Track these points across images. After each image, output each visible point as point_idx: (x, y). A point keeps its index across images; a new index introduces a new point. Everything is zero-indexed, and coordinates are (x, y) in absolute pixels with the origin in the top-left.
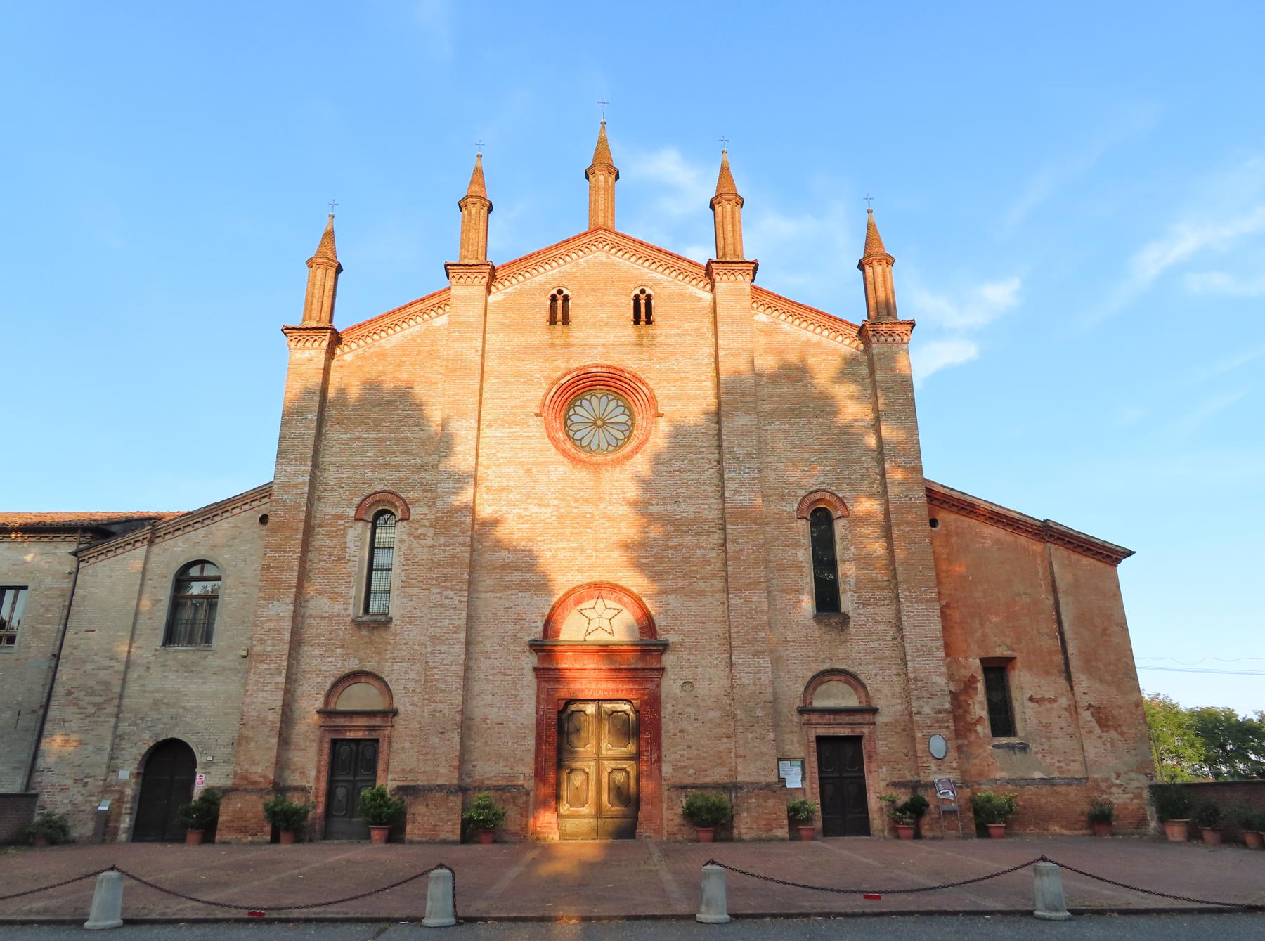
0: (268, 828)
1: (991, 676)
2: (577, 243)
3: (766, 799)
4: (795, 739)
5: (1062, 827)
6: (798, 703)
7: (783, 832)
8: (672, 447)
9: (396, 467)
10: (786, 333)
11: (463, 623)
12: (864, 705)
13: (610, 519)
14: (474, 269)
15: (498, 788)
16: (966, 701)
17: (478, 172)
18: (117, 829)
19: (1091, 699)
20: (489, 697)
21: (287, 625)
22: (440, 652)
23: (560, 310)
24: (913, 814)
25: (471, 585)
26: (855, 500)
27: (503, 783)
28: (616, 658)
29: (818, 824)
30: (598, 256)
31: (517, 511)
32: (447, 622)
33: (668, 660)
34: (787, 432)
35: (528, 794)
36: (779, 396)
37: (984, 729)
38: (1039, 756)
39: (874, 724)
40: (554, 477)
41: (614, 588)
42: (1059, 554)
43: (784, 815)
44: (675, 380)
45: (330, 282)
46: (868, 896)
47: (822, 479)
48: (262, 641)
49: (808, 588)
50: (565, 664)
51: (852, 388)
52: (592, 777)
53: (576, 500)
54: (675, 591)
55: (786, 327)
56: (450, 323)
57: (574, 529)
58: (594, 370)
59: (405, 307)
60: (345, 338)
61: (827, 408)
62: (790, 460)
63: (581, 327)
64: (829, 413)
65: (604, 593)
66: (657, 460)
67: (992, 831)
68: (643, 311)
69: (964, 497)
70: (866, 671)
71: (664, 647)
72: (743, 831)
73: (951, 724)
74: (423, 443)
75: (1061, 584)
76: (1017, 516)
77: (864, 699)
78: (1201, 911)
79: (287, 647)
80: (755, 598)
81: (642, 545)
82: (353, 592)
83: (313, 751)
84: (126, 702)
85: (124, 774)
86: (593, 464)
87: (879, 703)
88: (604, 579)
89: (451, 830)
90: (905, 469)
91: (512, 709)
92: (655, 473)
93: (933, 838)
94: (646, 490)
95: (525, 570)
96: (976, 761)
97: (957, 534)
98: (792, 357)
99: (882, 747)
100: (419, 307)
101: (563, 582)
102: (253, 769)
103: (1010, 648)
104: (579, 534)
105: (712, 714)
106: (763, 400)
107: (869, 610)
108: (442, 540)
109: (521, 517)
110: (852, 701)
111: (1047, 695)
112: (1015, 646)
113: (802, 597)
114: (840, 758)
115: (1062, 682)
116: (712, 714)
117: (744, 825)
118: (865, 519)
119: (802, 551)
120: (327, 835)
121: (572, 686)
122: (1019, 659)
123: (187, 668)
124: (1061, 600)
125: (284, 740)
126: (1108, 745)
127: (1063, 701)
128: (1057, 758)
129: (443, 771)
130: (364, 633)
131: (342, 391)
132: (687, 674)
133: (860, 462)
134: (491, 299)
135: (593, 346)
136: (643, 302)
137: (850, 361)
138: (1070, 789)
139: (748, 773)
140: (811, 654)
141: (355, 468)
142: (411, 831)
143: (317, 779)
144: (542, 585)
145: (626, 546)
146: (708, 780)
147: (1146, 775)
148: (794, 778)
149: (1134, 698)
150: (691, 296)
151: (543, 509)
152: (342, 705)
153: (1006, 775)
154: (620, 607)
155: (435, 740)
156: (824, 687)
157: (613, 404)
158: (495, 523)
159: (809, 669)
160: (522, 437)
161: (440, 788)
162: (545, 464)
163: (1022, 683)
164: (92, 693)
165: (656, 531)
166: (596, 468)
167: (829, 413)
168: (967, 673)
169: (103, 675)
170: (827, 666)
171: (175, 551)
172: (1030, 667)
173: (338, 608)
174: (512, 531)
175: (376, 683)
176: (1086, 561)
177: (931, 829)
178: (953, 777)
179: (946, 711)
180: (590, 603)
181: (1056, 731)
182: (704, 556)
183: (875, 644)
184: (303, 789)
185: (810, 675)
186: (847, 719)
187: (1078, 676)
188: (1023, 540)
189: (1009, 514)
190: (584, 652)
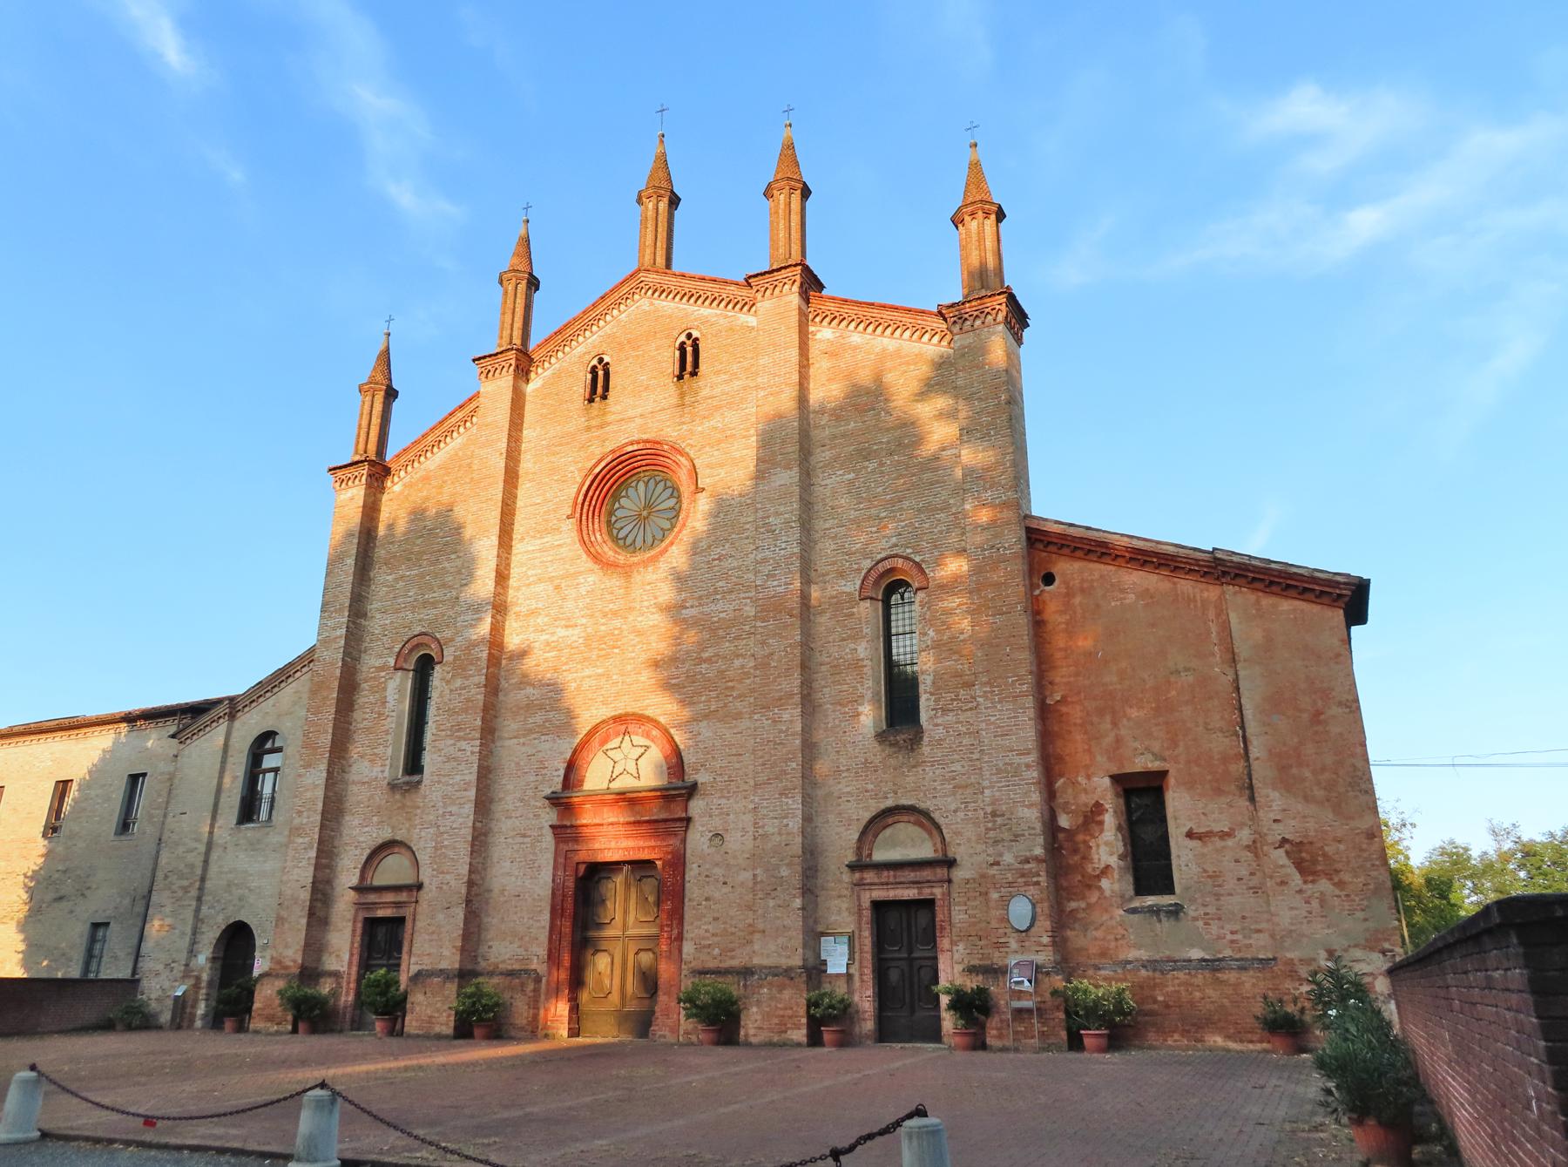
0: (290, 1018)
1: (1136, 800)
3: (781, 988)
4: (845, 906)
5: (1228, 1037)
6: (850, 857)
7: (800, 1035)
8: (713, 529)
9: (434, 605)
10: (855, 348)
11: (473, 777)
12: (939, 855)
13: (639, 633)
14: (501, 358)
15: (511, 974)
16: (1085, 842)
18: (193, 1015)
19: (1289, 830)
22: (451, 814)
23: (599, 383)
24: (973, 1007)
26: (938, 562)
27: (517, 967)
28: (638, 808)
29: (869, 1025)
31: (545, 637)
32: (458, 778)
33: (696, 806)
34: (851, 482)
35: (538, 980)
36: (843, 436)
37: (1116, 885)
38: (1200, 924)
39: (950, 881)
40: (583, 591)
41: (640, 719)
42: (1239, 600)
43: (802, 1011)
44: (720, 442)
47: (894, 540)
48: (300, 813)
49: (869, 695)
50: (585, 819)
51: (941, 402)
52: (618, 960)
54: (706, 716)
55: (856, 338)
58: (630, 448)
59: (446, 419)
61: (907, 434)
62: (853, 521)
64: (906, 446)
66: (695, 550)
67: (1087, 1041)
68: (689, 360)
69: (1090, 534)
70: (943, 806)
71: (692, 790)
72: (752, 1032)
73: (1043, 879)
75: (1242, 650)
76: (1171, 550)
77: (939, 846)
79: (319, 818)
80: (786, 717)
81: (674, 660)
84: (208, 884)
87: (958, 851)
88: (630, 710)
89: (446, 1024)
90: (993, 506)
91: (526, 878)
92: (694, 567)
93: (1004, 1049)
94: (680, 590)
95: (551, 704)
96: (1099, 934)
97: (1082, 590)
98: (864, 377)
99: (959, 916)
100: (460, 415)
101: (589, 715)
103: (1157, 757)
104: (607, 656)
107: (950, 717)
108: (458, 683)
109: (548, 644)
110: (926, 851)
111: (1216, 828)
112: (1167, 753)
113: (861, 709)
115: (1244, 803)
117: (753, 1024)
118: (948, 587)
119: (864, 644)
121: (591, 846)
122: (1172, 773)
123: (253, 846)
124: (1242, 673)
126: (1315, 904)
127: (1245, 835)
128: (1228, 927)
129: (446, 953)
130: (398, 797)
132: (717, 823)
135: (631, 419)
137: (942, 365)
138: (1245, 976)
140: (870, 787)
141: (397, 611)
142: (411, 1023)
143: (350, 964)
144: (566, 724)
145: (656, 664)
146: (735, 963)
147: (1384, 952)
148: (837, 959)
149: (1365, 824)
150: (742, 327)
151: (570, 631)
153: (1143, 954)
154: (647, 743)
155: (440, 917)
156: (888, 832)
158: (523, 654)
159: (866, 808)
160: (553, 547)
163: (1180, 806)
164: (181, 876)
165: (691, 637)
166: (626, 571)
167: (906, 446)
168: (1087, 800)
169: (191, 858)
170: (890, 803)
171: (250, 725)
172: (1190, 784)
173: (377, 769)
174: (539, 663)
175: (403, 850)
176: (1286, 605)
177: (1000, 1037)
180: (615, 743)
181: (1230, 884)
182: (743, 667)
183: (957, 767)
184: (336, 975)
185: (867, 816)
186: (911, 875)
187: (1262, 791)
188: (1186, 586)
190: (603, 803)
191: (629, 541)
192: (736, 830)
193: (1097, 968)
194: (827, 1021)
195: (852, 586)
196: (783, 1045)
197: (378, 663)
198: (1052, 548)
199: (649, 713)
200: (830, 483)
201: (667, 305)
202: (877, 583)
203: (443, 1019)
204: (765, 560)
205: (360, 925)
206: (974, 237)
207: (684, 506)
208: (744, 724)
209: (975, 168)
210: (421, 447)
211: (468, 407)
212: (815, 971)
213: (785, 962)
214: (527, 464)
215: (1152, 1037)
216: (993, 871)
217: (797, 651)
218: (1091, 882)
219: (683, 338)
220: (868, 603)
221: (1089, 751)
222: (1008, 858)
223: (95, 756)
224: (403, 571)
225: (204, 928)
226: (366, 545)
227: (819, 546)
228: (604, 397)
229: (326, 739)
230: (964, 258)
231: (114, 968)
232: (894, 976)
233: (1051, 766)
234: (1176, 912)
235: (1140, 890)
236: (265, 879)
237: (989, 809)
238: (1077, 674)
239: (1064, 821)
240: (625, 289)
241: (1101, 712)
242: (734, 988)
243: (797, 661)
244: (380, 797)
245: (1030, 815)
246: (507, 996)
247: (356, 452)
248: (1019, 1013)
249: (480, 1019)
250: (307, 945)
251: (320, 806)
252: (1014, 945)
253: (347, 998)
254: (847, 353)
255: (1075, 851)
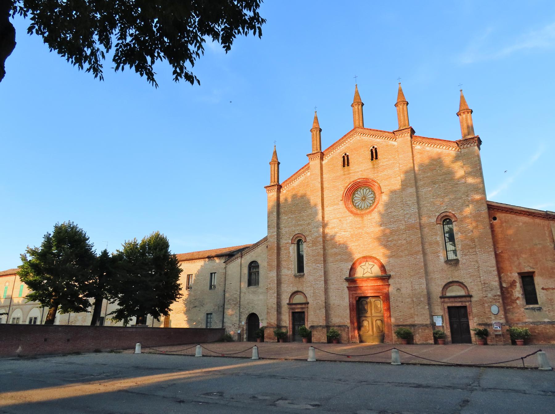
0: (276, 338)
2: (349, 135)
3: (425, 330)
4: (439, 308)
6: (440, 295)
7: (432, 341)
10: (428, 151)
11: (323, 274)
12: (467, 294)
13: (368, 233)
14: (316, 155)
15: (339, 326)
17: (316, 118)
18: (243, 338)
20: (334, 297)
21: (275, 278)
23: (346, 161)
24: (483, 335)
25: (325, 261)
29: (450, 339)
30: (357, 138)
35: (348, 328)
37: (521, 302)
38: (547, 312)
39: (471, 301)
40: (348, 221)
43: (432, 335)
44: (387, 179)
45: (276, 168)
46: (348, 356)
48: (270, 284)
53: (356, 228)
56: (311, 175)
57: (360, 237)
60: (283, 186)
63: (353, 166)
65: (368, 260)
67: (518, 343)
68: (374, 155)
70: (467, 281)
71: (389, 277)
73: (501, 301)
74: (308, 216)
78: (446, 365)
82: (293, 266)
83: (287, 316)
84: (241, 303)
85: (243, 323)
86: (360, 214)
87: (472, 293)
88: (367, 255)
89: (324, 339)
91: (341, 301)
95: (344, 252)
96: (517, 315)
97: (506, 222)
99: (474, 310)
100: (302, 170)
101: (357, 256)
102: (272, 321)
103: (532, 268)
105: (408, 300)
106: (425, 178)
107: (467, 257)
110: (462, 293)
111: (551, 287)
112: (534, 267)
114: (458, 315)
116: (408, 300)
117: (417, 338)
119: (439, 237)
120: (294, 340)
123: (254, 292)
125: (279, 312)
131: (286, 200)
133: (461, 198)
134: (324, 162)
135: (358, 172)
136: (374, 151)
139: (418, 320)
141: (290, 227)
142: (313, 339)
143: (289, 324)
146: (408, 323)
148: (439, 322)
150: (391, 145)
152: (294, 302)
153: (531, 320)
155: (318, 311)
156: (450, 288)
157: (368, 191)
160: (337, 209)
161: (320, 326)
162: (345, 217)
163: (539, 282)
164: (233, 301)
169: (235, 296)
170: (451, 280)
171: (247, 259)
172: (542, 275)
177: (491, 342)
178: (501, 321)
179: (498, 295)
180: (363, 264)
184: (285, 327)
185: (444, 284)
186: (459, 300)
188: (538, 221)
189: (529, 211)
191: (359, 207)
192: (403, 287)
193: (517, 324)
194: (438, 338)
195: (434, 220)
196: (427, 344)
197: (286, 242)
198: (495, 210)
199: (374, 256)
200: (423, 191)
201: (366, 138)
202: (441, 219)
203: (324, 338)
204: (407, 214)
205: (291, 314)
206: (465, 120)
207: (377, 196)
208: (403, 259)
209: (462, 98)
210: (290, 180)
211: (307, 167)
212: (433, 325)
213: (425, 323)
214: (325, 185)
215: (535, 341)
216: (485, 299)
217: (420, 239)
218: (514, 301)
219: (372, 148)
220: (439, 225)
221: (511, 266)
222: (490, 295)
223: (199, 268)
224: (290, 215)
225: (242, 315)
226: (278, 210)
227: (422, 209)
228: (348, 165)
229: (275, 263)
230: (462, 126)
231: (216, 324)
232: (455, 326)
233: (500, 270)
234: (540, 309)
235: (528, 303)
236: (262, 302)
237: (483, 282)
238: (505, 245)
239: (504, 285)
240: (352, 133)
241: (513, 255)
242: (412, 330)
243: (420, 242)
244: (292, 279)
245: (496, 284)
246: (339, 332)
247: (271, 182)
248: (496, 335)
249: (334, 338)
250: (277, 319)
251: (276, 282)
252: (493, 318)
253: (290, 333)
254: (425, 152)
255: (508, 293)
